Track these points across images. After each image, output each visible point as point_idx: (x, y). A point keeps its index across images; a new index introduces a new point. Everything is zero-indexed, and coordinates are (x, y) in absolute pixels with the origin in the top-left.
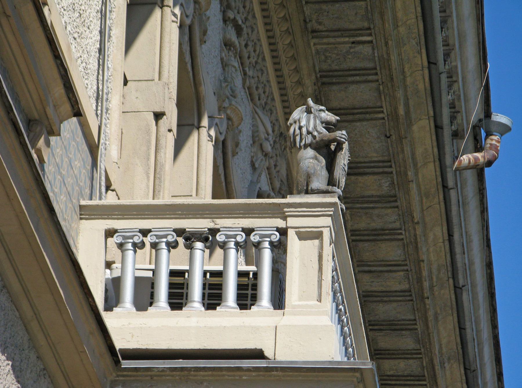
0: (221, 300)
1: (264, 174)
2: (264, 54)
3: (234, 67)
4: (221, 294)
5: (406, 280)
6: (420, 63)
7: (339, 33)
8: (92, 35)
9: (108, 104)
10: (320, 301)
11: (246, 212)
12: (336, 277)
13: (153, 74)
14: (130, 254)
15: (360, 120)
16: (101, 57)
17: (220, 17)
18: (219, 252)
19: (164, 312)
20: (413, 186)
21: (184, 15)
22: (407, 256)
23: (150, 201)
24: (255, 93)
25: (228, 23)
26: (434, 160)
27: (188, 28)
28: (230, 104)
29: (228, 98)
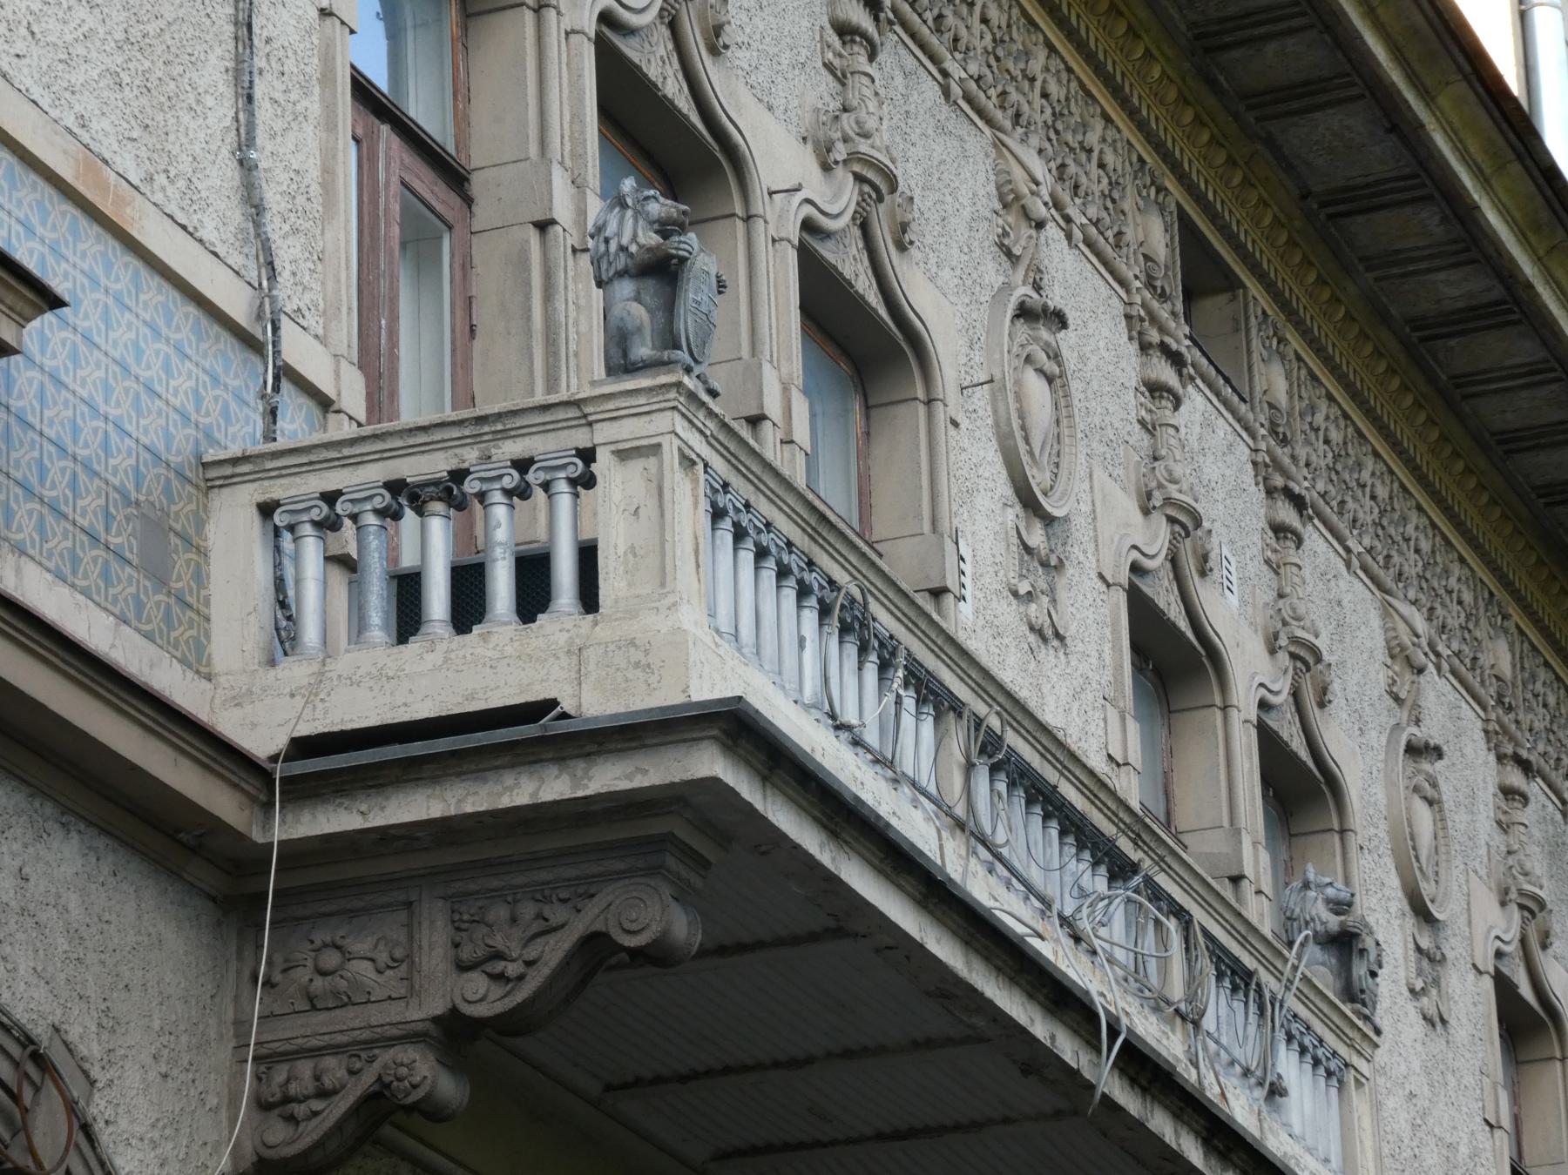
14: (564, 501)
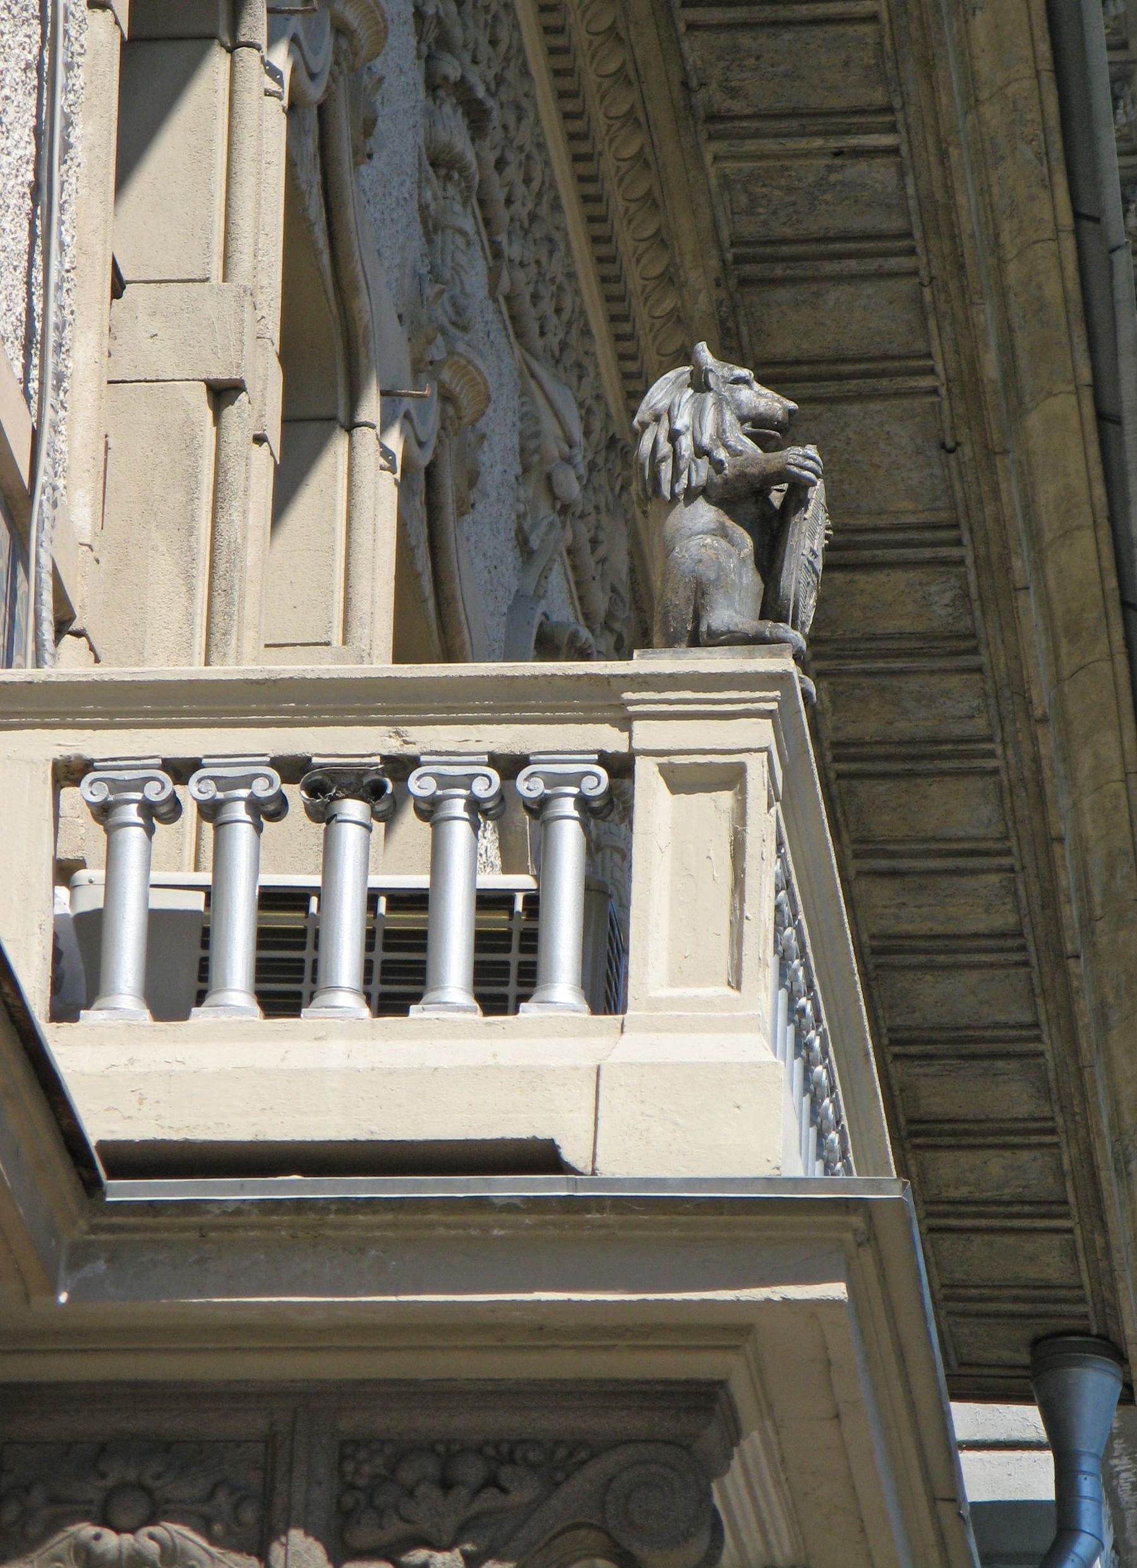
0: (423, 983)
1: (557, 568)
2: (556, 190)
3: (462, 232)
4: (424, 962)
5: (1007, 900)
6: (1047, 215)
7: (793, 124)
8: (9, 143)
9: (64, 359)
10: (738, 987)
11: (505, 704)
12: (786, 909)
13: (207, 260)
14: (133, 837)
15: (859, 397)
16: (39, 212)
17: (417, 75)
18: (410, 822)
19: (241, 1022)
20: (1029, 605)
21: (303, 74)
22: (1010, 824)
23: (194, 669)
24: (530, 314)
25: (442, 93)
26: (1095, 522)
27: (315, 112)
28: (451, 352)
29: (444, 332)
